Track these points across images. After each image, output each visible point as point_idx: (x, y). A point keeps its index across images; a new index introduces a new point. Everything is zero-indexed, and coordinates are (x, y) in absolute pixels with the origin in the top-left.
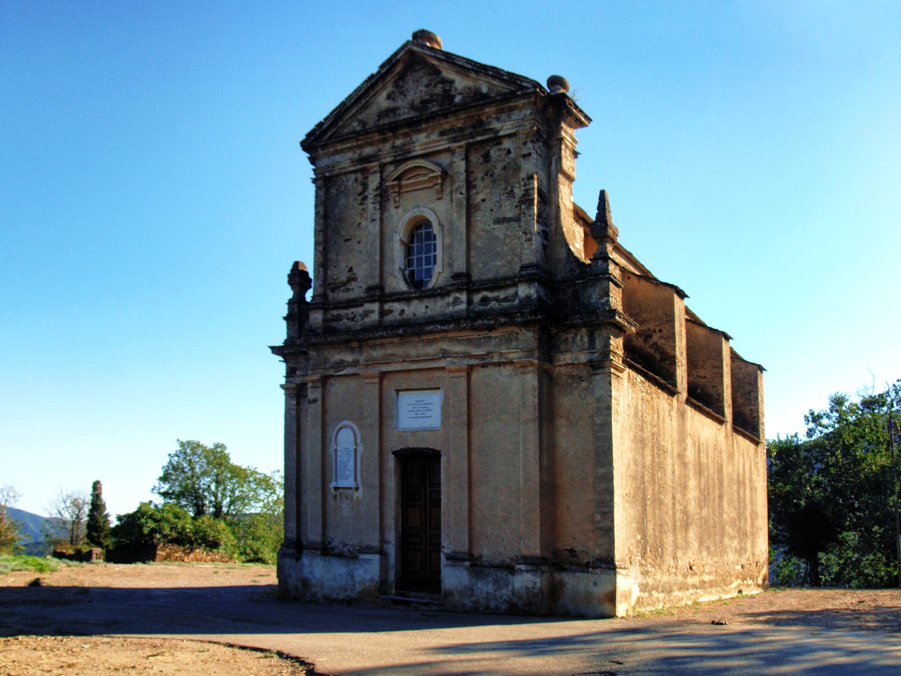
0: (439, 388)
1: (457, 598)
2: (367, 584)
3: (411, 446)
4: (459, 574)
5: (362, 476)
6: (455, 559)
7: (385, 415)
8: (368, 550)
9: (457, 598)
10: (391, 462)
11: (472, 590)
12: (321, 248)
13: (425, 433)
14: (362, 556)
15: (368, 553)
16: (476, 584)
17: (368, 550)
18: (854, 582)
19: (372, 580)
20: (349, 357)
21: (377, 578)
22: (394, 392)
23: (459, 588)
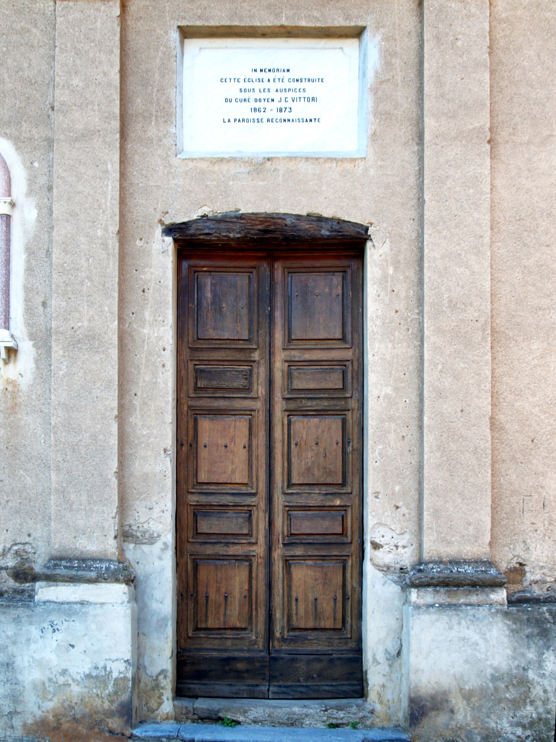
0: (358, 33)
1: (463, 714)
2: (76, 689)
3: (246, 209)
4: (472, 634)
5: (29, 310)
6: (447, 582)
7: (138, 104)
8: (72, 568)
9: (463, 714)
10: (160, 260)
11: (523, 683)
12: (274, 216)
13: (303, 166)
14: (45, 592)
15: (73, 580)
16: (540, 664)
17: (72, 568)
18: (109, 580)
19: (98, 678)
20: (243, 246)
21: (119, 669)
22: (175, 35)
23: (473, 682)
